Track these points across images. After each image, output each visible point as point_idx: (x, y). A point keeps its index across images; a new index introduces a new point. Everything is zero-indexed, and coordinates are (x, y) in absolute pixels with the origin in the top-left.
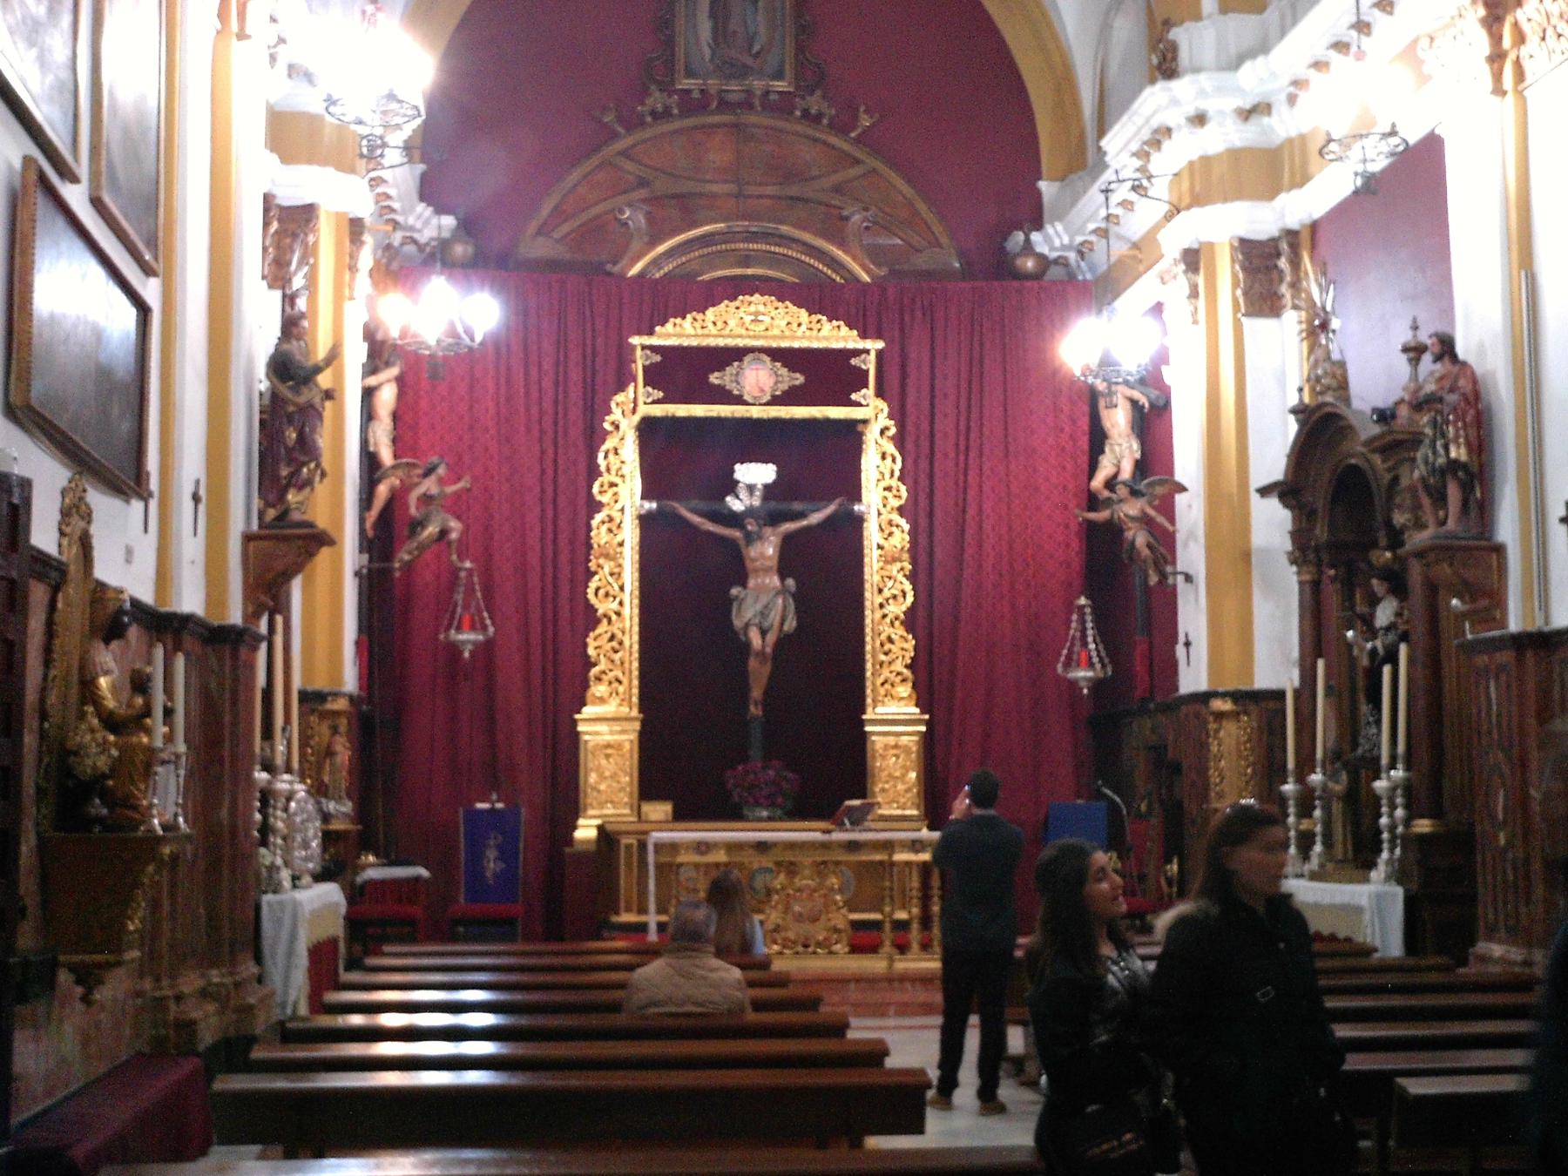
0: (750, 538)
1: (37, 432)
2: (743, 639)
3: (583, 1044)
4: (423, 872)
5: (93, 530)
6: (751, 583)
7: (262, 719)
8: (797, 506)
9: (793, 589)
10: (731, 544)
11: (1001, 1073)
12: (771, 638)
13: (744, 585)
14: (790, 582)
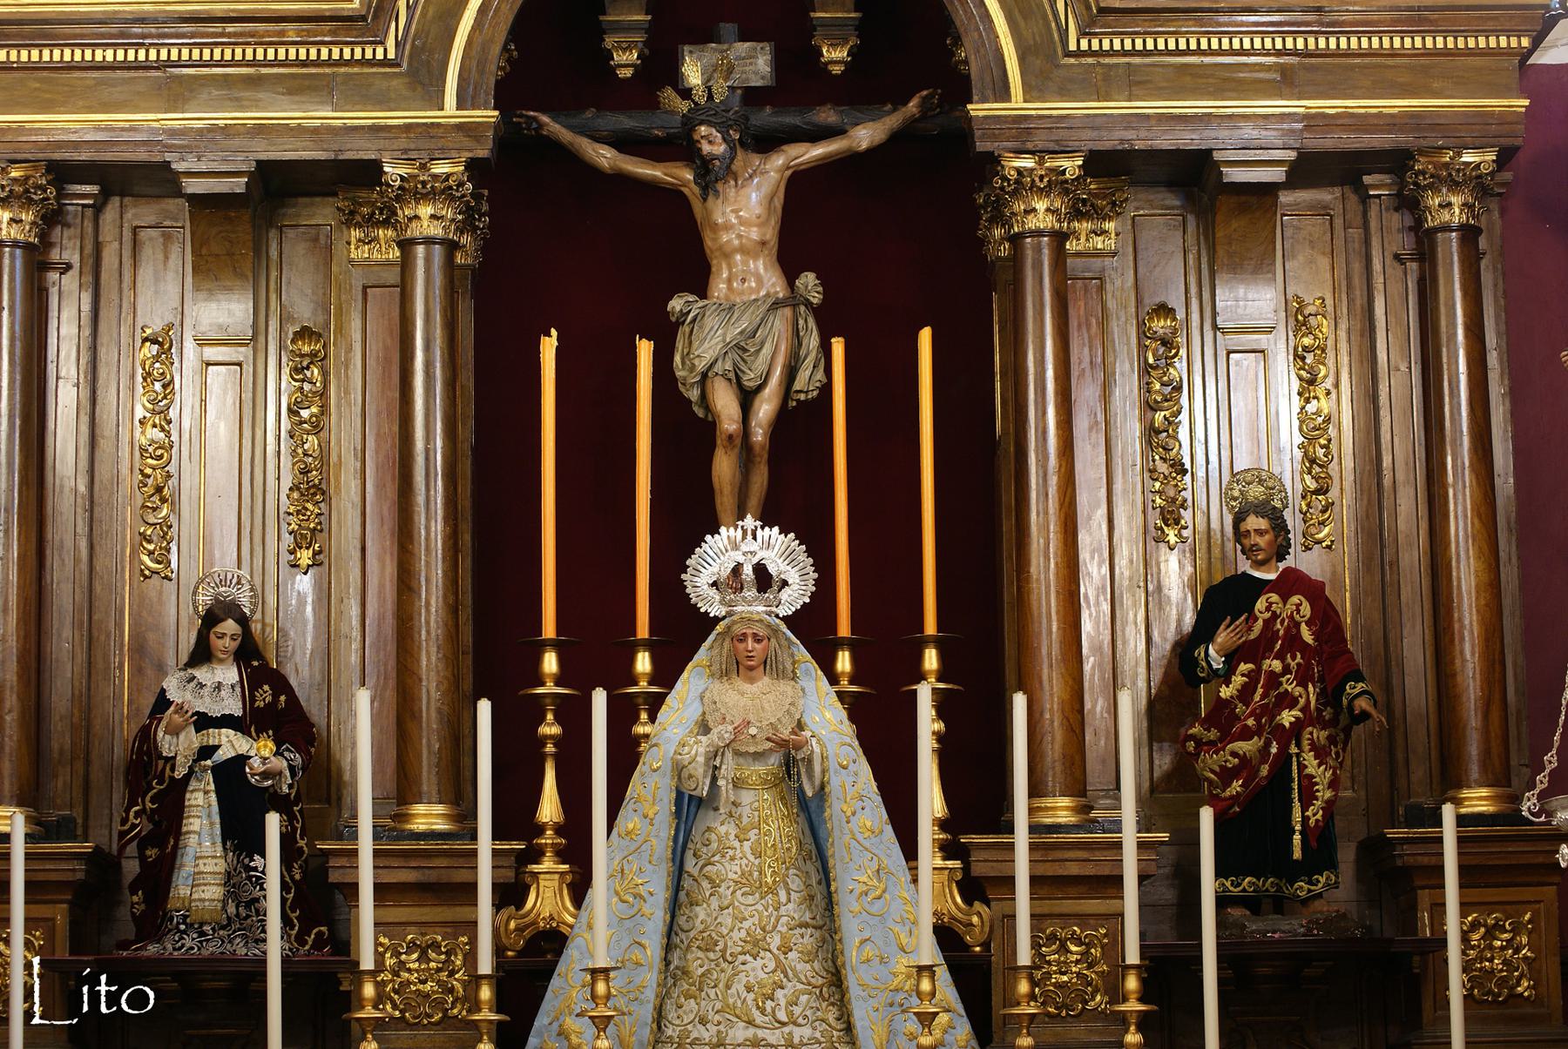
0: (710, 176)
1: (1062, 515)
2: (700, 413)
3: (1382, 413)
4: (549, 347)
5: (832, 690)
6: (719, 288)
7: (374, 774)
8: (827, 115)
9: (816, 298)
10: (673, 197)
11: (702, 655)
12: (765, 409)
13: (701, 289)
14: (809, 282)
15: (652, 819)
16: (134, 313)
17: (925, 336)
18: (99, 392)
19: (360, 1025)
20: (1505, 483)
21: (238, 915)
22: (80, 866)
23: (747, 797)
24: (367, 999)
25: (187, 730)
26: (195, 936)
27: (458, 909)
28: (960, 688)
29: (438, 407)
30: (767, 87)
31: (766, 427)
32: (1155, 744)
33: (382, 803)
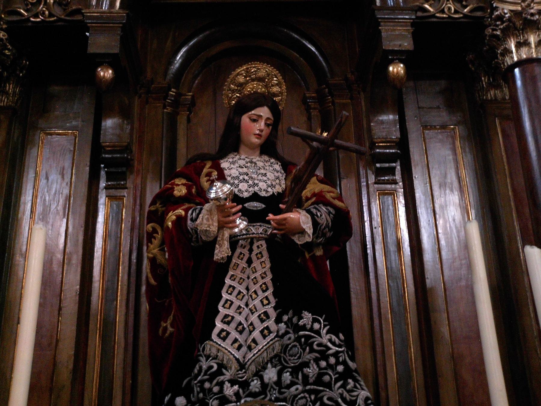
15: (276, 183)
16: (215, 116)
17: (183, 386)
20: (402, 252)
21: (279, 382)
23: (240, 187)
24: (303, 389)
28: (280, 310)
30: (260, 149)
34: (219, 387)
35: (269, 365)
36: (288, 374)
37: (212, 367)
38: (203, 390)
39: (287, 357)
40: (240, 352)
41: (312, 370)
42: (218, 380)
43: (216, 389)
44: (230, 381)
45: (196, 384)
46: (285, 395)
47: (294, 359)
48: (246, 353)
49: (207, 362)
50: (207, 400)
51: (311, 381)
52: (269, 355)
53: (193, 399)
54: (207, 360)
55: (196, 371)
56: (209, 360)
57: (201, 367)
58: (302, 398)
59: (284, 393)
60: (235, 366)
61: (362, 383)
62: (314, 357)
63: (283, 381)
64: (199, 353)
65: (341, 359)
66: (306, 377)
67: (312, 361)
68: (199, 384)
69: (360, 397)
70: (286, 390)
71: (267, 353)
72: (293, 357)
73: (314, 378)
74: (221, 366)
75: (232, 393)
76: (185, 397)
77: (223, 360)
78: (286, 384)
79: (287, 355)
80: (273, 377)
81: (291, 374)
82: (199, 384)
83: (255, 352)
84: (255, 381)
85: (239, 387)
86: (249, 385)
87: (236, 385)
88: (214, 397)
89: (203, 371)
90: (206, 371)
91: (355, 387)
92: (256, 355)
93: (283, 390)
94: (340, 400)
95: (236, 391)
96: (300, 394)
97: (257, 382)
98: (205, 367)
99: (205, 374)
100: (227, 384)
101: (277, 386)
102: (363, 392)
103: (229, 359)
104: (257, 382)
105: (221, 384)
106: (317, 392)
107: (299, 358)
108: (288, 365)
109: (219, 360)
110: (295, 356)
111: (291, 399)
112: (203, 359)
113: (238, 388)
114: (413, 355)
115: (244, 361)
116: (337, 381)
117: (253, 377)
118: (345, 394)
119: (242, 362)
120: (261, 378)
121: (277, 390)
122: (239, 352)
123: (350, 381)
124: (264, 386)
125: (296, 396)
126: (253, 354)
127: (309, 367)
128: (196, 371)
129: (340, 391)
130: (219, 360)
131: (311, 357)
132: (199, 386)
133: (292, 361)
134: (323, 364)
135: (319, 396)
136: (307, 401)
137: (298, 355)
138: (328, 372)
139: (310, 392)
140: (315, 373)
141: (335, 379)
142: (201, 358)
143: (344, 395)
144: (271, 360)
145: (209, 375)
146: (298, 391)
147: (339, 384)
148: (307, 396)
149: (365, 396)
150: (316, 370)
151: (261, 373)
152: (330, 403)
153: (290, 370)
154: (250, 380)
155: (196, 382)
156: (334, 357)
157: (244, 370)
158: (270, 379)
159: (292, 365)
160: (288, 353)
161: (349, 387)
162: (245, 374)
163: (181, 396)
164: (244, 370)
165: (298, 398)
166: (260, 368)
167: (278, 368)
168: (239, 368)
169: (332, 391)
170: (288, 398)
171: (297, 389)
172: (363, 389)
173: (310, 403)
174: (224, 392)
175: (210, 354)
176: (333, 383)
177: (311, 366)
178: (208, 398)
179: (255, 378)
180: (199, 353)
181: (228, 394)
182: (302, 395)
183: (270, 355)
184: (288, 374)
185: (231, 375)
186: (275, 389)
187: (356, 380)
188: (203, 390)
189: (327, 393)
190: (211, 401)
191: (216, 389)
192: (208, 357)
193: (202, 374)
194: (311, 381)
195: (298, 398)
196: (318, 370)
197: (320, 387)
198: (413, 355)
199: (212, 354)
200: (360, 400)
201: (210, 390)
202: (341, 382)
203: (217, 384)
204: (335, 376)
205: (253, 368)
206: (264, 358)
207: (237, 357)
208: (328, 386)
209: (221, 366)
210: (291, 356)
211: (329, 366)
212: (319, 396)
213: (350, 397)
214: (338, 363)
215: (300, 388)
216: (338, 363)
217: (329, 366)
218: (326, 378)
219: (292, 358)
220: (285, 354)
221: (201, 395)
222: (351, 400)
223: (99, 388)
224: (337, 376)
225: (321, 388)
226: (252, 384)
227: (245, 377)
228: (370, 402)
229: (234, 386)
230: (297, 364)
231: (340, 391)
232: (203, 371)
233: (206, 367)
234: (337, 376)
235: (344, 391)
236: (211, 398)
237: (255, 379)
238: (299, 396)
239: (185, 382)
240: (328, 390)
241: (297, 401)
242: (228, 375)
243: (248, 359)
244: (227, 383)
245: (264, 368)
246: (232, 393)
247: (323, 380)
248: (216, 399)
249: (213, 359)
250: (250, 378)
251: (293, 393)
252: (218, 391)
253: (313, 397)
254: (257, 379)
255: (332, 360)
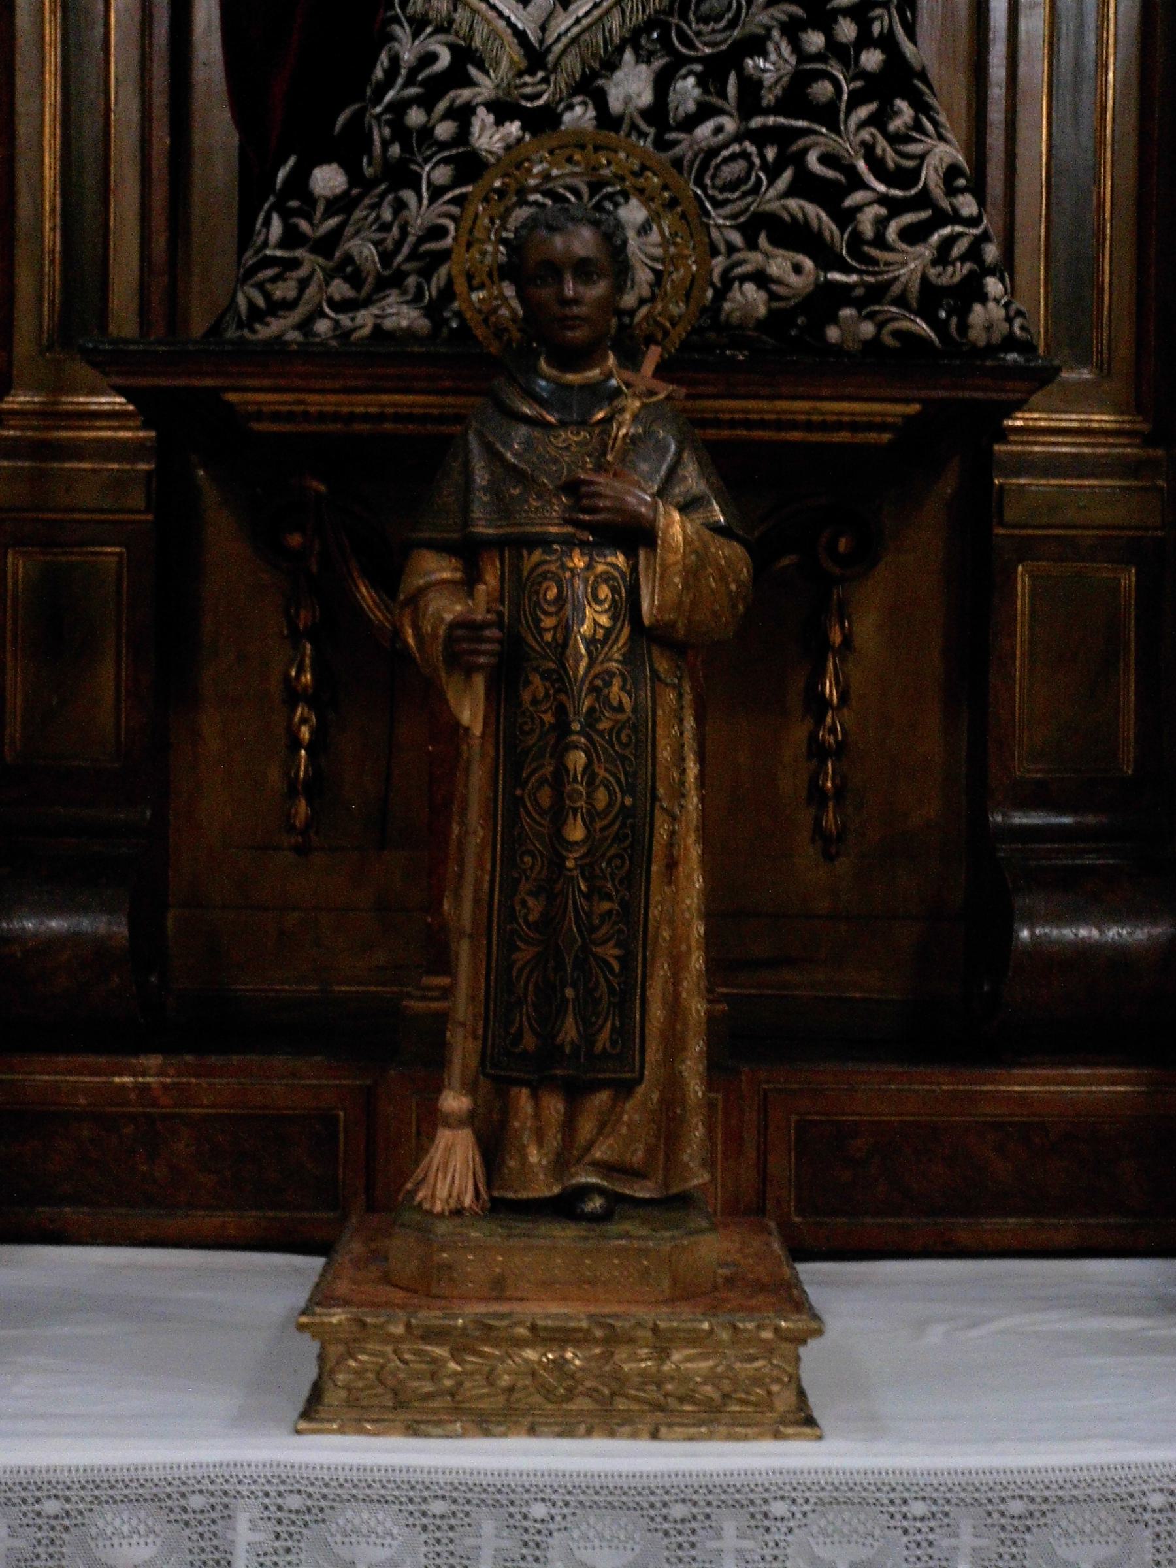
18: (1020, 109)
19: (721, 234)
21: (657, 113)
22: (900, 419)
25: (802, 1277)
26: (442, 174)
27: (824, 440)
29: (877, 407)
31: (1004, 84)
32: (508, 1294)
33: (661, 586)
34: (452, 166)
35: (628, 56)
36: (691, 80)
37: (433, 57)
38: (401, 132)
39: (689, 24)
40: (530, 9)
41: (774, 64)
42: (453, 101)
43: (444, 130)
44: (490, 106)
45: (378, 117)
46: (677, 150)
47: (713, 31)
48: (550, 15)
49: (417, 42)
50: (414, 167)
51: (768, 98)
52: (627, 21)
53: (369, 171)
54: (415, 35)
55: (379, 74)
56: (422, 37)
57: (395, 60)
58: (733, 157)
59: (676, 143)
60: (511, 53)
61: (942, 118)
62: (785, 18)
63: (672, 106)
64: (389, 14)
65: (876, 28)
66: (751, 87)
67: (776, 34)
68: (388, 116)
69: (932, 161)
70: (681, 136)
71: (623, 12)
72: (712, 24)
73: (778, 91)
74: (464, 55)
75: (498, 147)
76: (342, 165)
77: (472, 38)
78: (681, 112)
79: (692, 17)
80: (639, 96)
81: (701, 82)
82: (388, 116)
83: (581, 13)
84: (579, 110)
85: (524, 128)
86: (556, 120)
87: (512, 120)
88: (439, 157)
89: (404, 71)
90: (414, 71)
91: (918, 126)
92: (585, 22)
93: (672, 136)
94: (861, 165)
95: (512, 140)
96: (726, 145)
97: (584, 114)
98: (408, 56)
99: (409, 82)
100: (484, 116)
101: (650, 124)
102: (941, 148)
103: (495, 34)
104: (584, 114)
105: (463, 115)
106: (781, 137)
107: (732, 25)
108: (692, 53)
109: (457, 34)
110: (718, 19)
111: (697, 162)
112: (402, 32)
113: (520, 133)
114: (1110, 92)
115: (541, 42)
116: (856, 100)
117: (571, 96)
118: (882, 145)
119: (537, 45)
120: (599, 99)
121: (650, 139)
122: (525, 7)
123: (902, 104)
124: (607, 120)
125: (713, 152)
126: (573, 18)
127: (764, 54)
128: (379, 74)
129: (865, 135)
130: (457, 34)
131: (773, 18)
132: (388, 123)
133: (706, 38)
134: (815, 40)
135: (794, 148)
136: (751, 165)
137: (730, 15)
138: (829, 68)
139: (762, 137)
140: (783, 71)
141: (850, 93)
142: (397, 29)
143: (879, 151)
144: (633, 39)
145: (422, 84)
146: (721, 137)
147: (863, 112)
148: (751, 148)
149: (948, 160)
150: (786, 61)
151: (601, 82)
152: (829, 173)
153: (698, 68)
154: (561, 106)
155: (378, 110)
156: (852, 19)
157: (541, 74)
158: (628, 100)
159: (707, 50)
160: (695, 14)
161: (895, 125)
162: (544, 86)
163: (329, 162)
164: (541, 74)
165: (719, 159)
166: (596, 66)
167: (658, 63)
168: (523, 65)
169: (838, 132)
170: (687, 158)
171: (719, 129)
172: (941, 138)
173: (761, 174)
174: (473, 140)
175: (426, 14)
176: (843, 106)
177: (771, 47)
178: (420, 160)
179: (577, 99)
180: (389, 14)
181: (486, 146)
182: (736, 148)
183: (631, 20)
184: (691, 80)
185: (498, 86)
186: (642, 135)
187: (921, 106)
188: (401, 132)
189: (821, 139)
190: (427, 168)
191: (444, 130)
192: (418, 25)
193: (400, 81)
194: (768, 98)
195: (719, 159)
196: (793, 60)
197: (797, 118)
198: (1110, 92)
199: (432, 14)
200: (932, 171)
201: (426, 132)
202: (873, 107)
203: (449, 114)
204: (852, 86)
205: (572, 64)
206: (610, 30)
207: (520, 26)
208: (828, 115)
209: (464, 55)
210: (704, 19)
211: (835, 49)
212: (794, 148)
213: (898, 159)
214: (864, 40)
215: (730, 124)
216: (864, 40)
217: (835, 49)
218: (822, 90)
219: (706, 29)
220: (684, 16)
221: (395, 150)
222: (898, 167)
223: (62, 156)
224: (859, 84)
225: (801, 123)
226: (568, 117)
227: (545, 97)
228: (962, 182)
229: (507, 124)
230: (723, 47)
231: (865, 135)
232: (404, 71)
233: (412, 58)
234: (859, 84)
235: (880, 138)
236: (427, 160)
237: (580, 103)
238: (725, 153)
239: (342, 119)
240: (824, 130)
241: (718, 167)
242: (485, 86)
243: (556, 35)
244: (482, 112)
245: (611, 65)
246: (498, 145)
247: (808, 95)
248: (446, 161)
249: (439, 30)
250: (561, 100)
251: (704, 144)
252: (453, 138)
253: (771, 153)
254: (584, 103)
255: (847, 30)
